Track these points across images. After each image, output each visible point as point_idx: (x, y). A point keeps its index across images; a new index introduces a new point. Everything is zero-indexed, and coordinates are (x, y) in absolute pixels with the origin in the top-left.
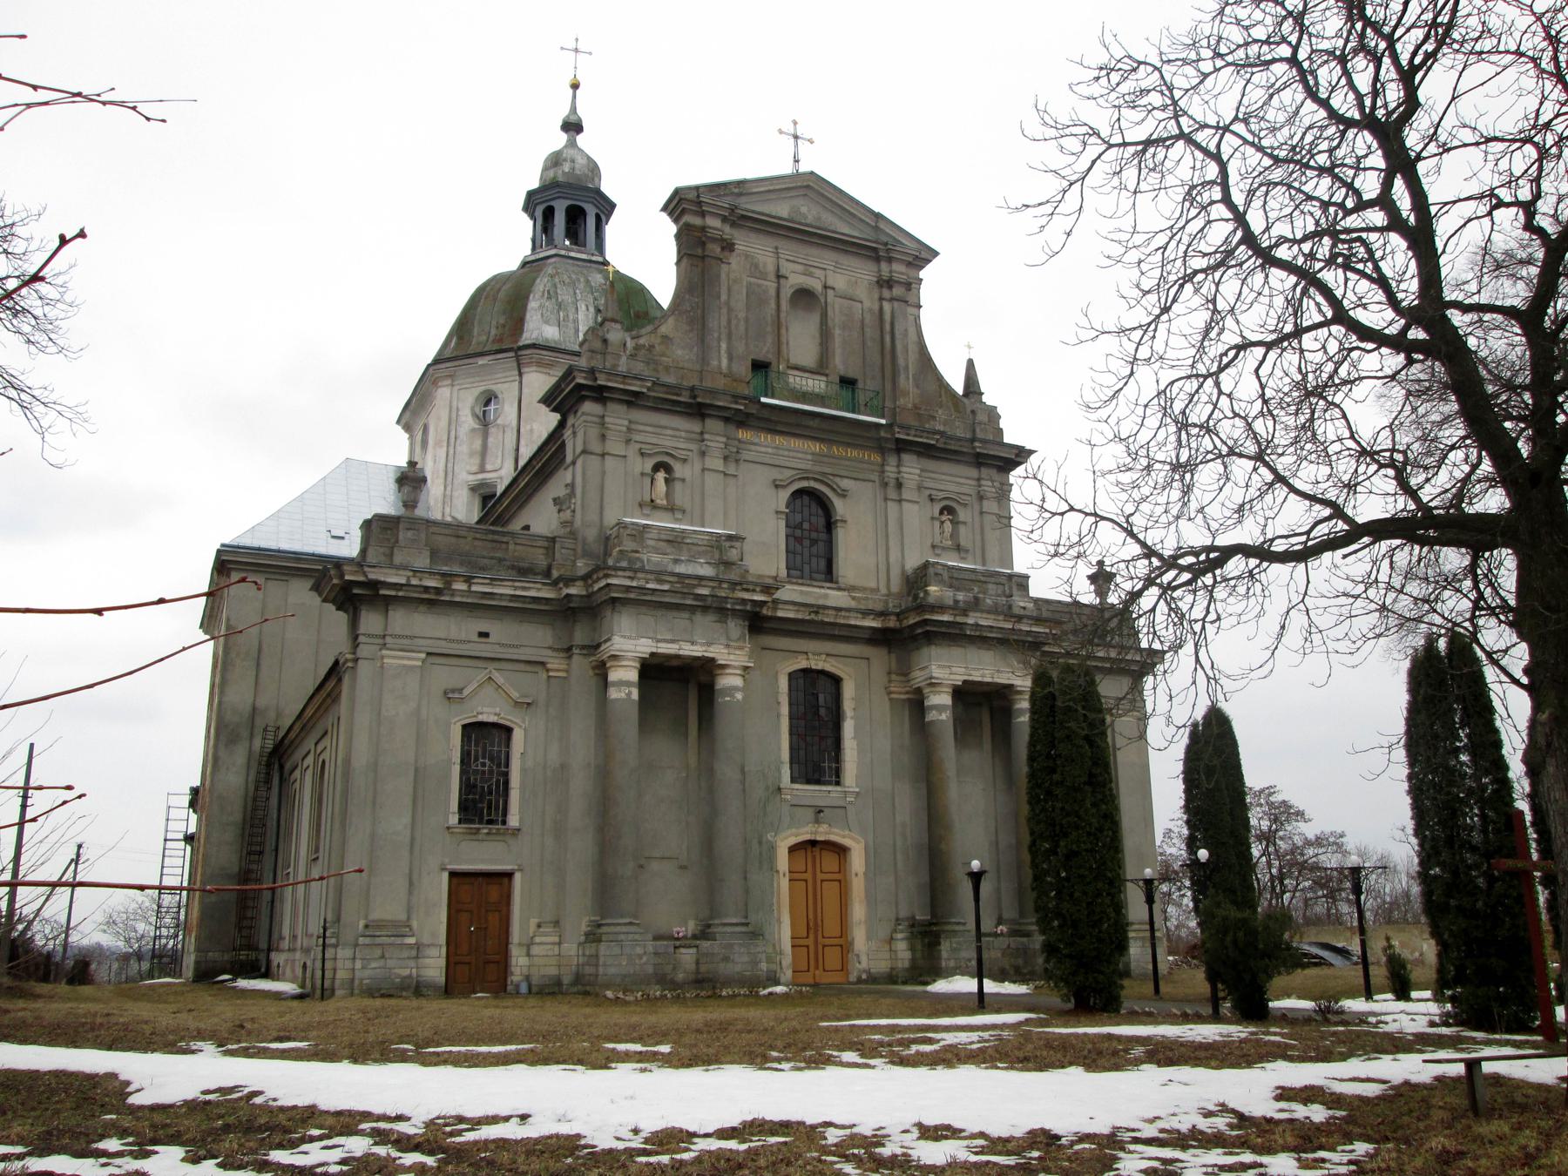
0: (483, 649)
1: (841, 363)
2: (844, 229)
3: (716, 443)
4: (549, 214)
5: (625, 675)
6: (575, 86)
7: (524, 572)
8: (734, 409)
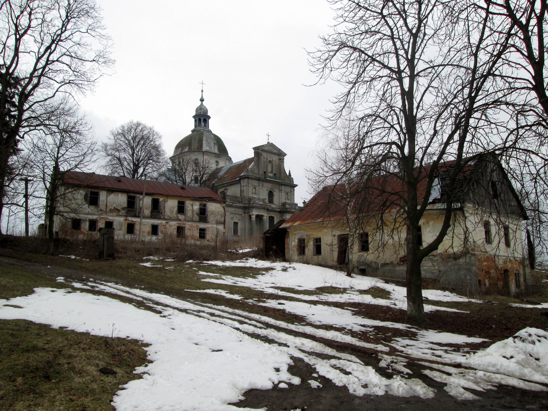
0: (236, 212)
1: (274, 172)
2: (275, 151)
3: (261, 184)
4: (200, 120)
5: (254, 217)
6: (202, 91)
7: (239, 202)
8: (262, 179)
